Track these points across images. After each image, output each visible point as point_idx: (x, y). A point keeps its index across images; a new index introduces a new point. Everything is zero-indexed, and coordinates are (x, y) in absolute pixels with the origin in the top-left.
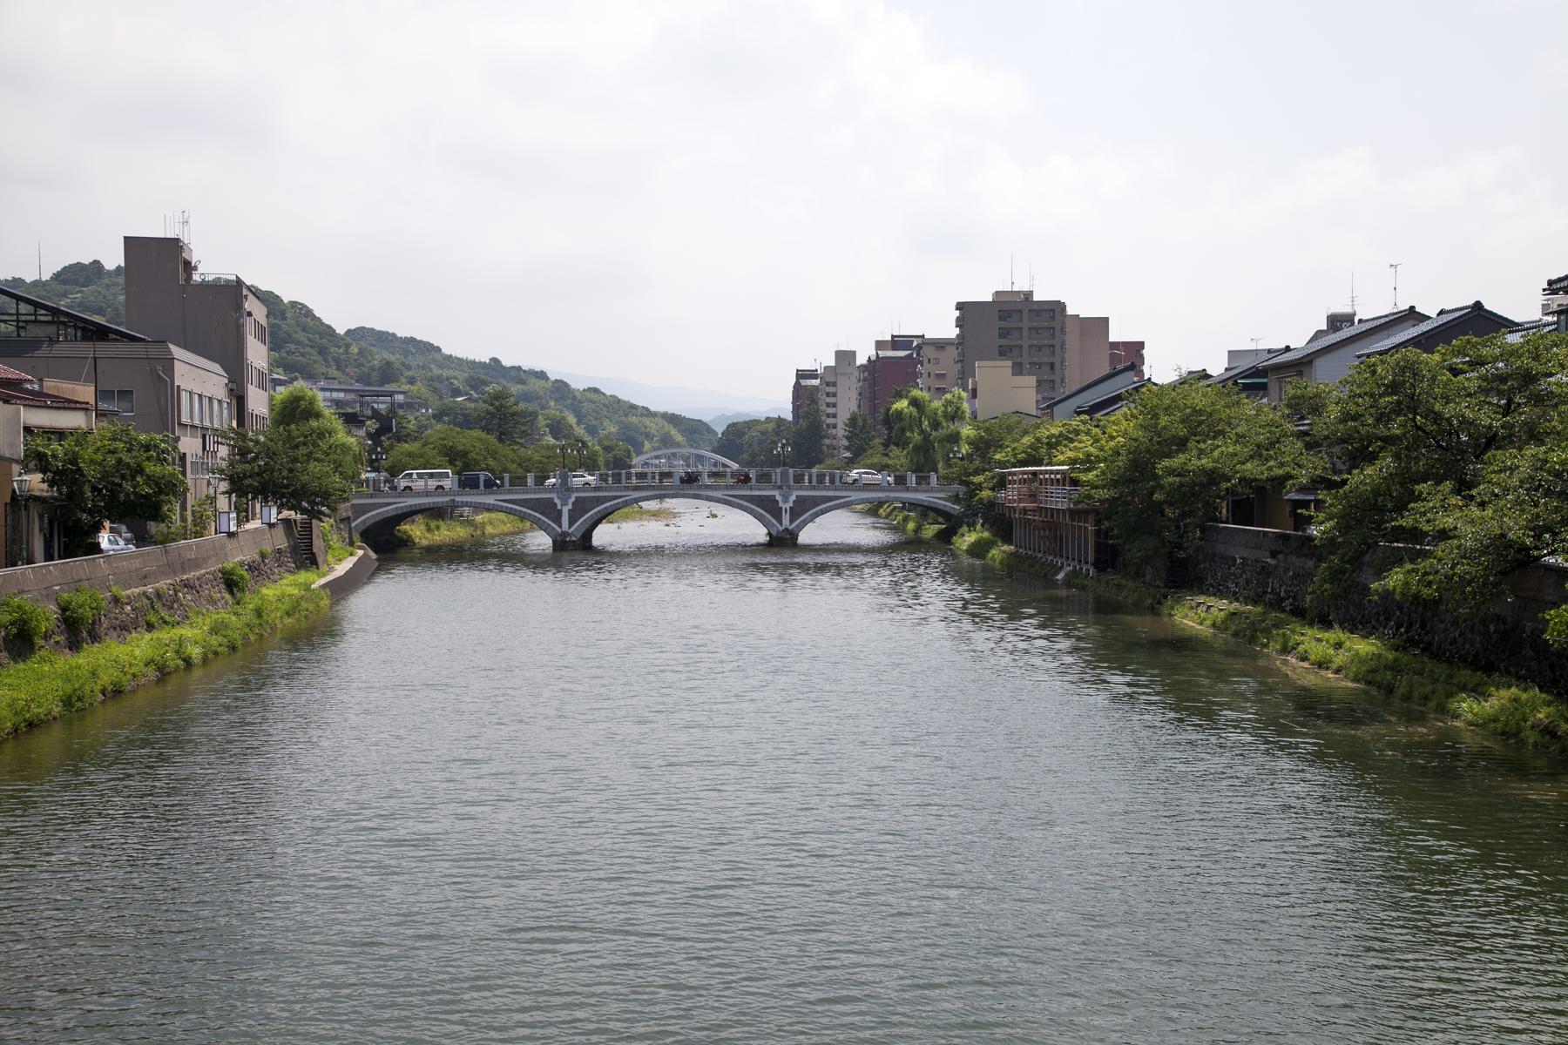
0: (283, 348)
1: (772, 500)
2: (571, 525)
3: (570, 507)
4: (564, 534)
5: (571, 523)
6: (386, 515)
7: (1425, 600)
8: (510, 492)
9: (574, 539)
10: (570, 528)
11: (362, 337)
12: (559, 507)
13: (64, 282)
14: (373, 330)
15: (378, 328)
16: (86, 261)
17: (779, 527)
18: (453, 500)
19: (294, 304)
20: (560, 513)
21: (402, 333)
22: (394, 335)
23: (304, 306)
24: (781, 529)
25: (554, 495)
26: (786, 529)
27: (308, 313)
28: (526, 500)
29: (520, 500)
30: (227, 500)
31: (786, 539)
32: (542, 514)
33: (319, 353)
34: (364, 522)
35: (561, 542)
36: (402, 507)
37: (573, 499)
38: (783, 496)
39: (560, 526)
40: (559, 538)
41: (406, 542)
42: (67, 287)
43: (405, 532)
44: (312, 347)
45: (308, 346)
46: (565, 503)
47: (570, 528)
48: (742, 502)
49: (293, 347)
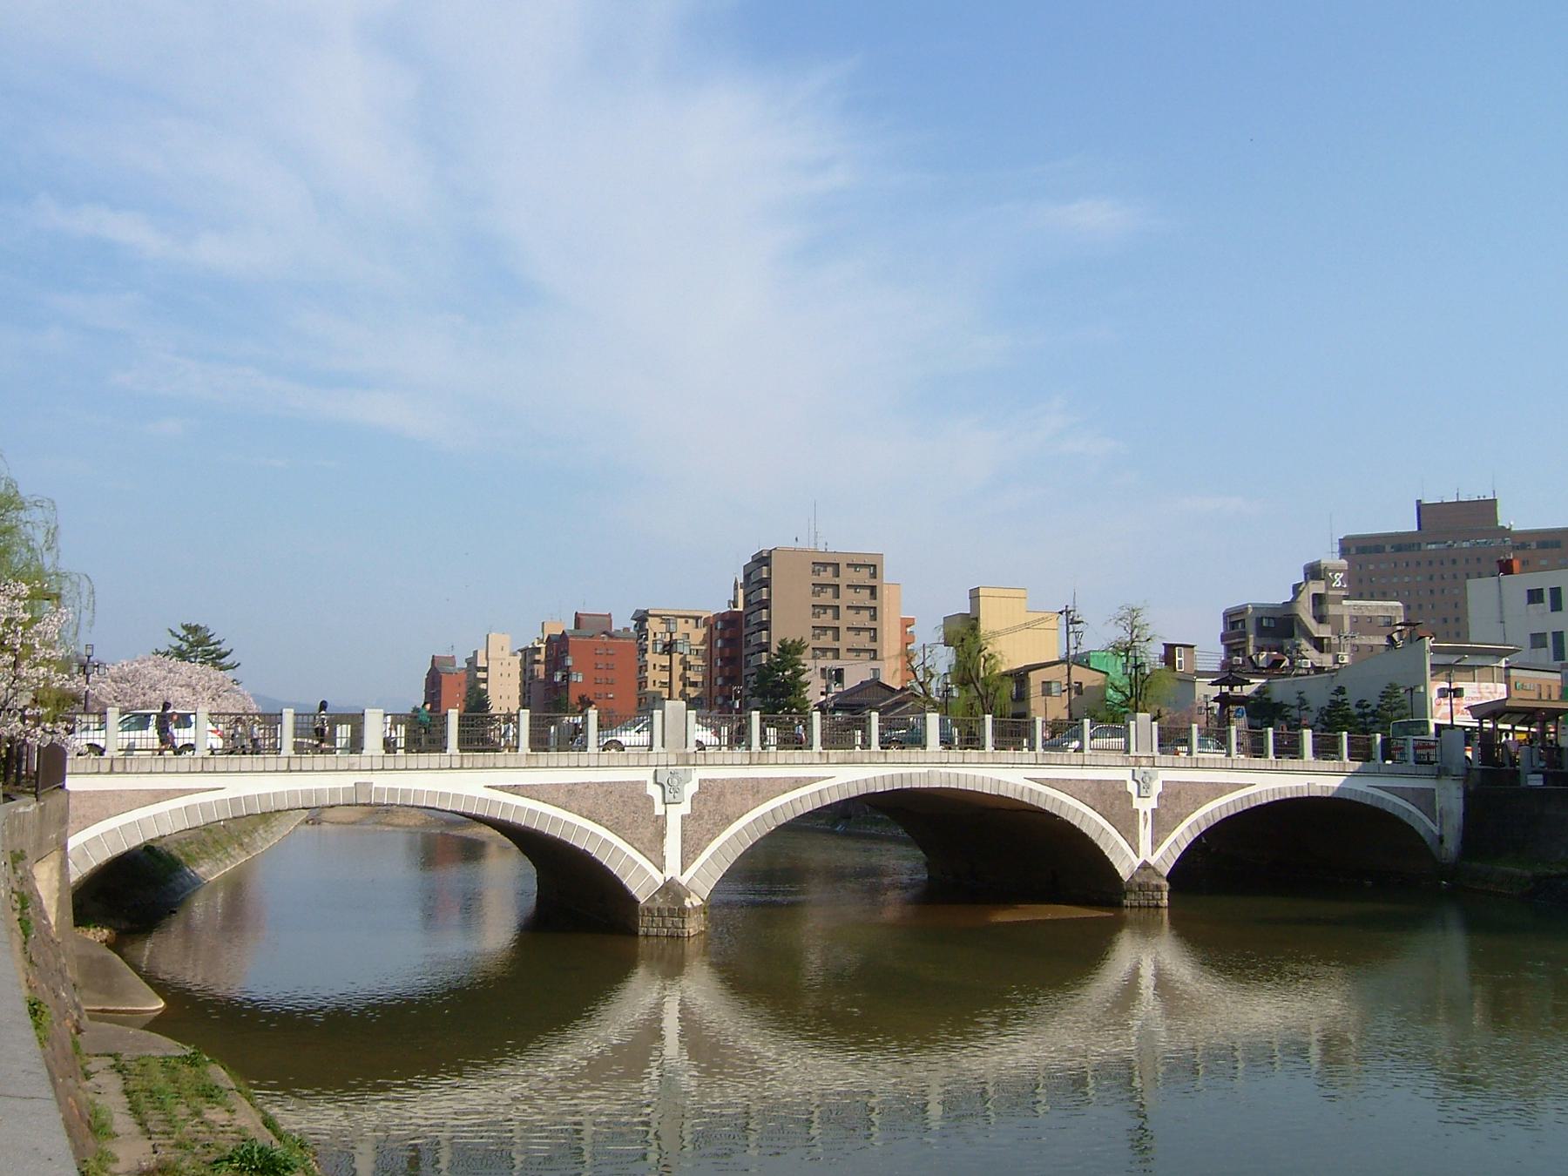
3: (685, 808)
12: (659, 809)
28: (571, 789)
47: (683, 869)
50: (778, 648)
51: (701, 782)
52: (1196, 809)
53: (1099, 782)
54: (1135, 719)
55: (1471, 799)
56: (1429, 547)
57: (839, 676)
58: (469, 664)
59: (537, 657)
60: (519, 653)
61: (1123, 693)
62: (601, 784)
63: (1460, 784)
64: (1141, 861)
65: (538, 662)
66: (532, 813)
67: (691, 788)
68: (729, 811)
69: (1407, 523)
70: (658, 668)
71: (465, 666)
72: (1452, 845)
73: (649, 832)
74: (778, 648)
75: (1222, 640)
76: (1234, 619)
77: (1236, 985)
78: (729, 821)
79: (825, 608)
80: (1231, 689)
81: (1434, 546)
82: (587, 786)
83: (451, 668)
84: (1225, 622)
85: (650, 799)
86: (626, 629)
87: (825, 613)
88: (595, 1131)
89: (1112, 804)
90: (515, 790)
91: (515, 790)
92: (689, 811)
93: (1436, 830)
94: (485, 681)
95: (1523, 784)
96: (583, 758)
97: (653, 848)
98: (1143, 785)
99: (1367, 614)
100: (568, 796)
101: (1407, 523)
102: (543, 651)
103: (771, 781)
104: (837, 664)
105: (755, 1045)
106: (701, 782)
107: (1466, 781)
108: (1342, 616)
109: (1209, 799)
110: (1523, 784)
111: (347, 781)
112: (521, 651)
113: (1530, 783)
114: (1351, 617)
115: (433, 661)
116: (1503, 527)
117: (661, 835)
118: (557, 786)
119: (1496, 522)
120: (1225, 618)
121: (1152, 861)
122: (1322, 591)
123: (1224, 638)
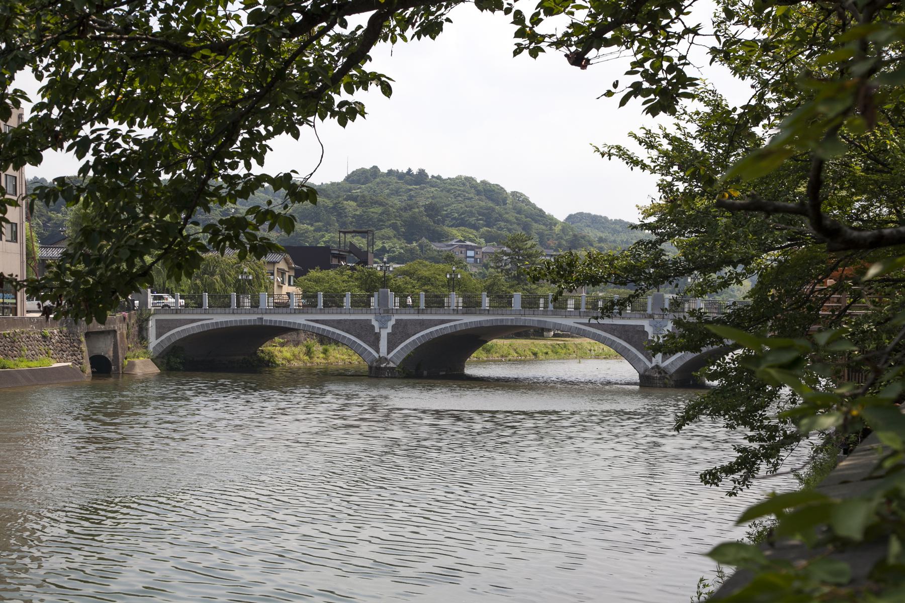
0: (495, 225)
1: (641, 331)
2: (390, 350)
3: (389, 330)
4: (382, 359)
5: (391, 348)
6: (197, 331)
7: (754, 463)
8: (321, 312)
9: (392, 365)
10: (388, 353)
11: (580, 220)
12: (377, 330)
13: (353, 182)
14: (589, 214)
15: (593, 213)
16: (368, 166)
17: (648, 363)
18: (261, 319)
19: (514, 194)
20: (377, 337)
21: (612, 216)
22: (605, 218)
23: (522, 195)
24: (650, 366)
25: (371, 317)
26: (657, 366)
27: (526, 201)
28: (339, 321)
29: (333, 321)
30: (634, 381)
31: (654, 378)
32: (358, 337)
33: (523, 229)
34: (169, 338)
35: (376, 367)
36: (207, 325)
37: (393, 322)
38: (655, 327)
39: (378, 351)
40: (375, 364)
41: (268, 364)
42: (352, 185)
43: (270, 354)
44: (518, 224)
45: (514, 223)
46: (383, 326)
47: (388, 353)
48: (603, 334)
49: (502, 224)
50: (55, 201)
51: (396, 320)
66: (324, 330)
74: (55, 201)
77: (515, 393)
82: (345, 321)
85: (373, 326)
90: (317, 321)
91: (317, 321)
92: (390, 331)
95: (185, 210)
105: (860, 461)
106: (396, 320)
111: (255, 317)
116: (21, 68)
119: (550, 222)
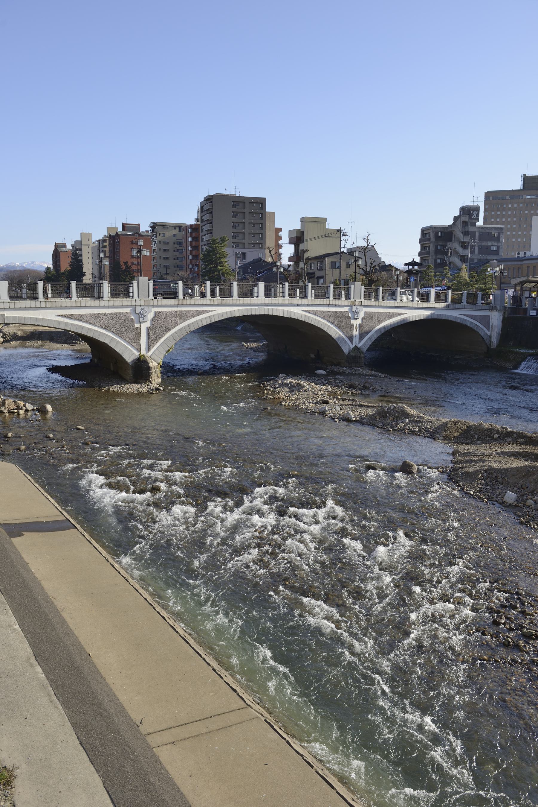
3: (148, 324)
28: (97, 316)
51: (155, 313)
52: (380, 324)
53: (336, 312)
54: (354, 285)
55: (505, 321)
56: (527, 197)
57: (244, 255)
58: (73, 247)
59: (105, 244)
60: (97, 242)
61: (362, 269)
62: (111, 314)
63: (501, 314)
64: (354, 346)
65: (105, 247)
67: (151, 316)
68: (169, 326)
69: (517, 185)
70: (162, 251)
71: (71, 248)
72: (495, 340)
73: (132, 335)
75: (420, 242)
76: (426, 232)
78: (168, 329)
79: (239, 223)
80: (413, 267)
81: (529, 197)
82: (104, 315)
83: (64, 249)
84: (422, 234)
86: (147, 231)
87: (238, 226)
88: (407, 634)
89: (342, 321)
93: (489, 333)
94: (81, 255)
96: (101, 302)
97: (135, 340)
98: (355, 313)
99: (487, 231)
100: (95, 320)
101: (517, 185)
102: (108, 241)
103: (189, 312)
104: (244, 250)
107: (504, 313)
108: (475, 232)
109: (386, 319)
110: (528, 315)
112: (97, 241)
113: (531, 314)
114: (479, 232)
115: (55, 246)
117: (138, 335)
118: (91, 315)
120: (422, 232)
121: (359, 346)
122: (467, 220)
123: (420, 241)
